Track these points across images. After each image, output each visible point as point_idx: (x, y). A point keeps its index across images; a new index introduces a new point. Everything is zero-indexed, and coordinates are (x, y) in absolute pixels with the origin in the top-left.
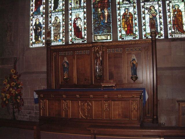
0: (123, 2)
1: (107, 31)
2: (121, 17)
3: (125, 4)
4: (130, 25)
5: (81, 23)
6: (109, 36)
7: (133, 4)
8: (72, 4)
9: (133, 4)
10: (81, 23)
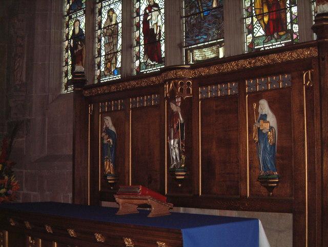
10: (160, 16)
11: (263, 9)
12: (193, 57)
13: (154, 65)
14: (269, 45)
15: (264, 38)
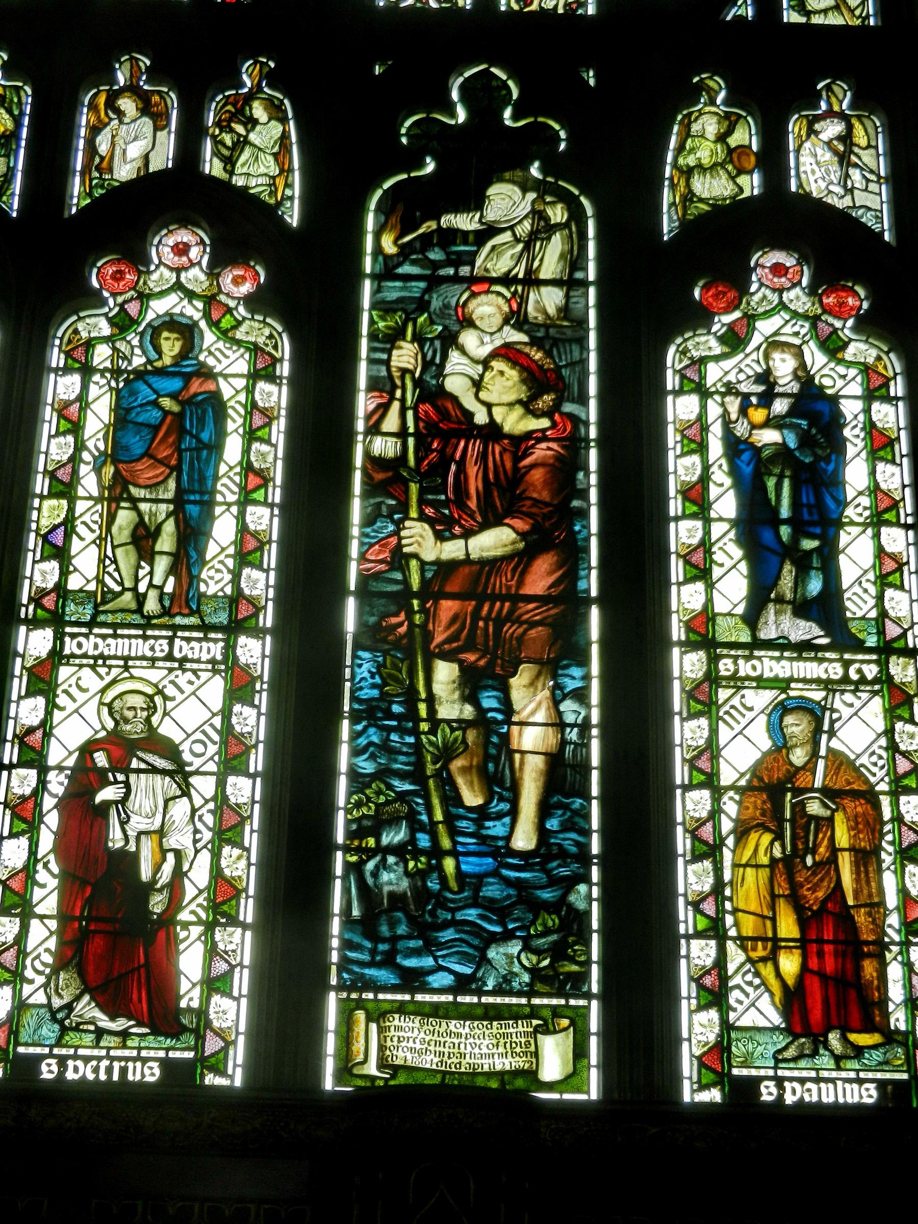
0: (752, 618)
1: (534, 971)
2: (731, 807)
3: (781, 645)
4: (845, 917)
5: (180, 809)
6: (545, 1029)
7: (884, 665)
8: (76, 545)
9: (884, 665)
10: (180, 809)
11: (774, 920)
12: (382, 1048)
13: (124, 1035)
14: (805, 1074)
15: (781, 1041)
